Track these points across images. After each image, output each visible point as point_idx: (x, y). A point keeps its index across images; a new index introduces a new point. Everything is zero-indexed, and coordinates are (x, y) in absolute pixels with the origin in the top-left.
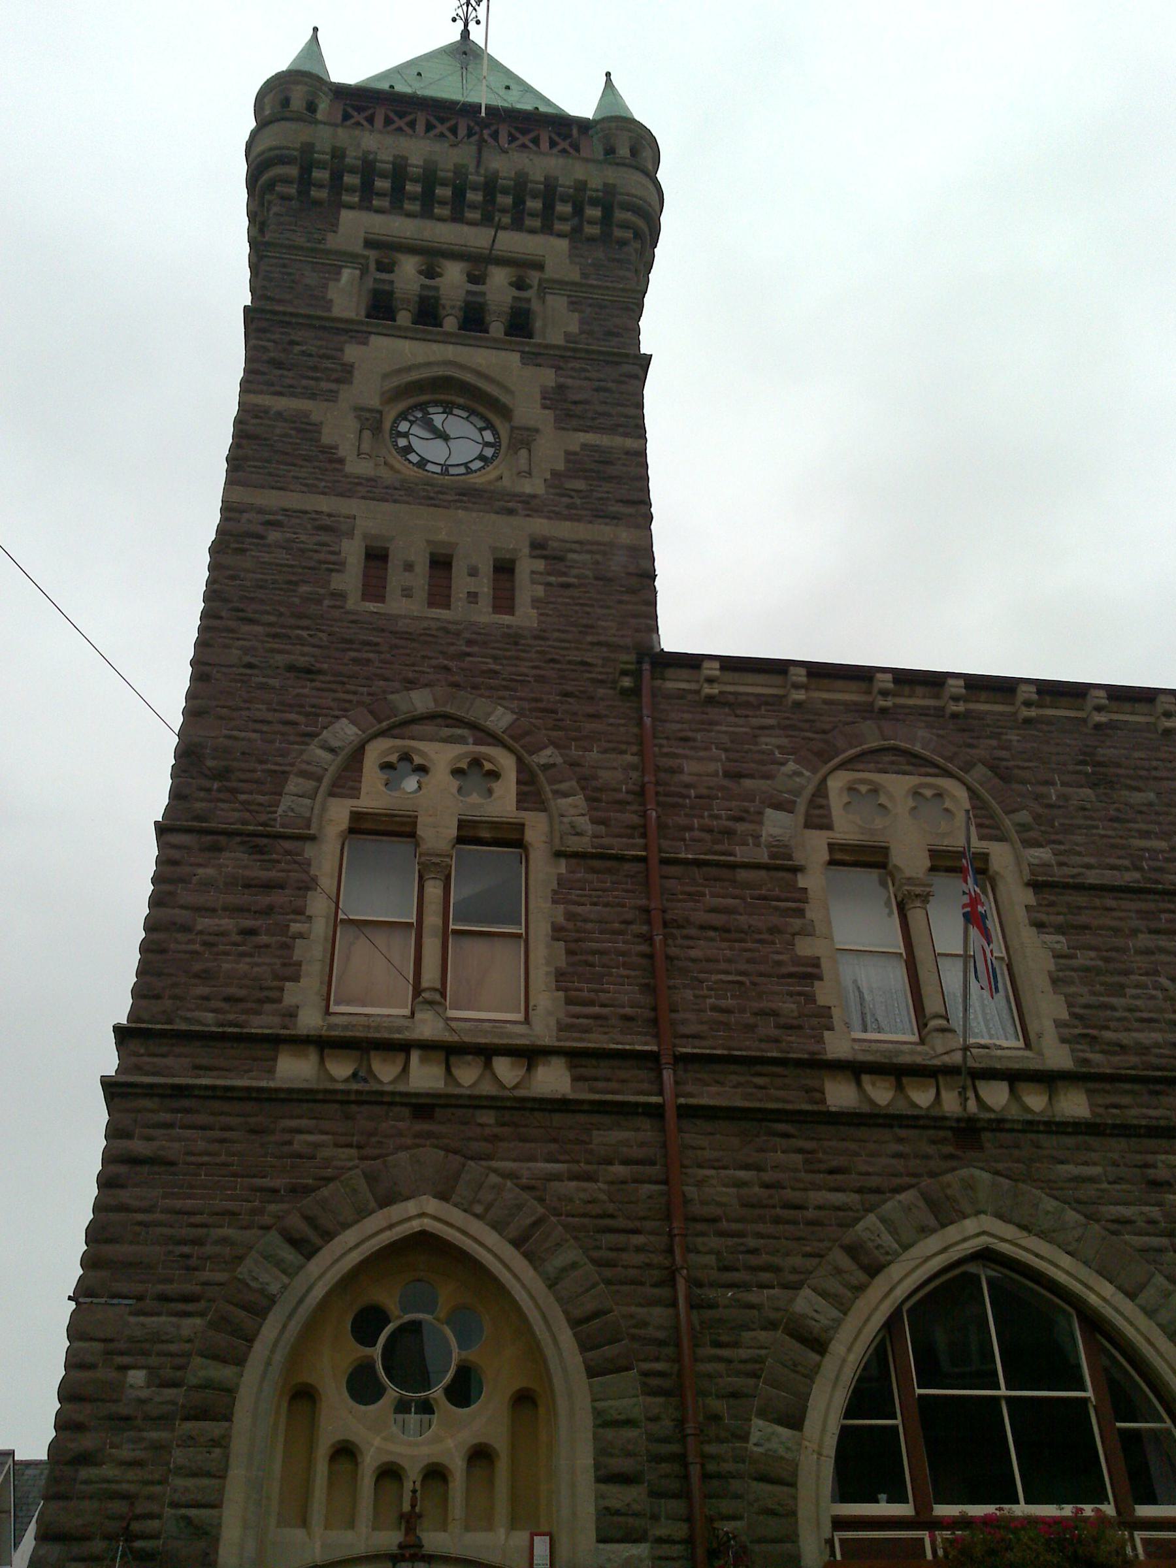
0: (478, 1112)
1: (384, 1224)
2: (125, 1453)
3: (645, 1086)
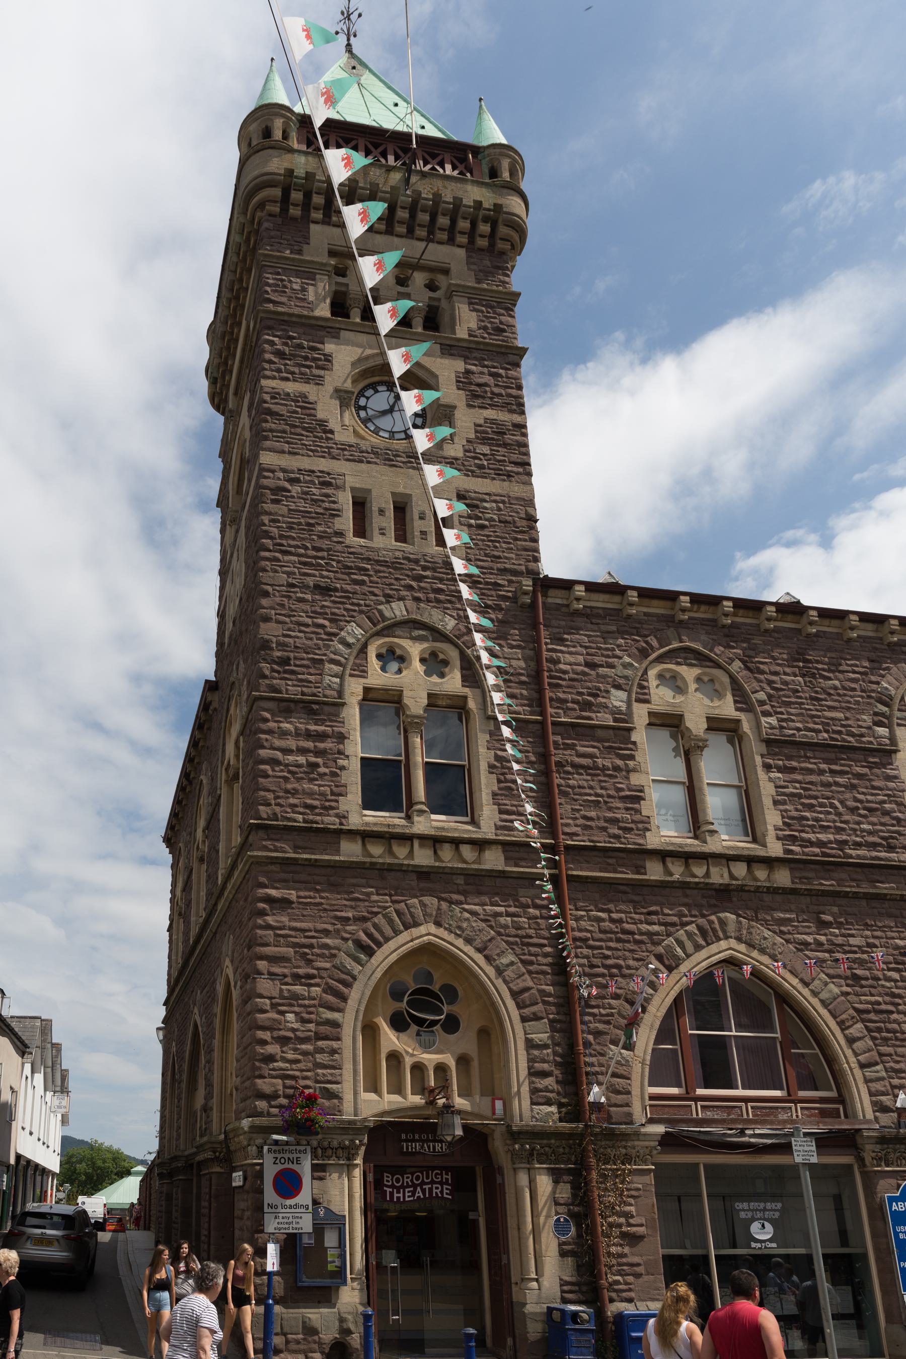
0: (454, 877)
1: (409, 939)
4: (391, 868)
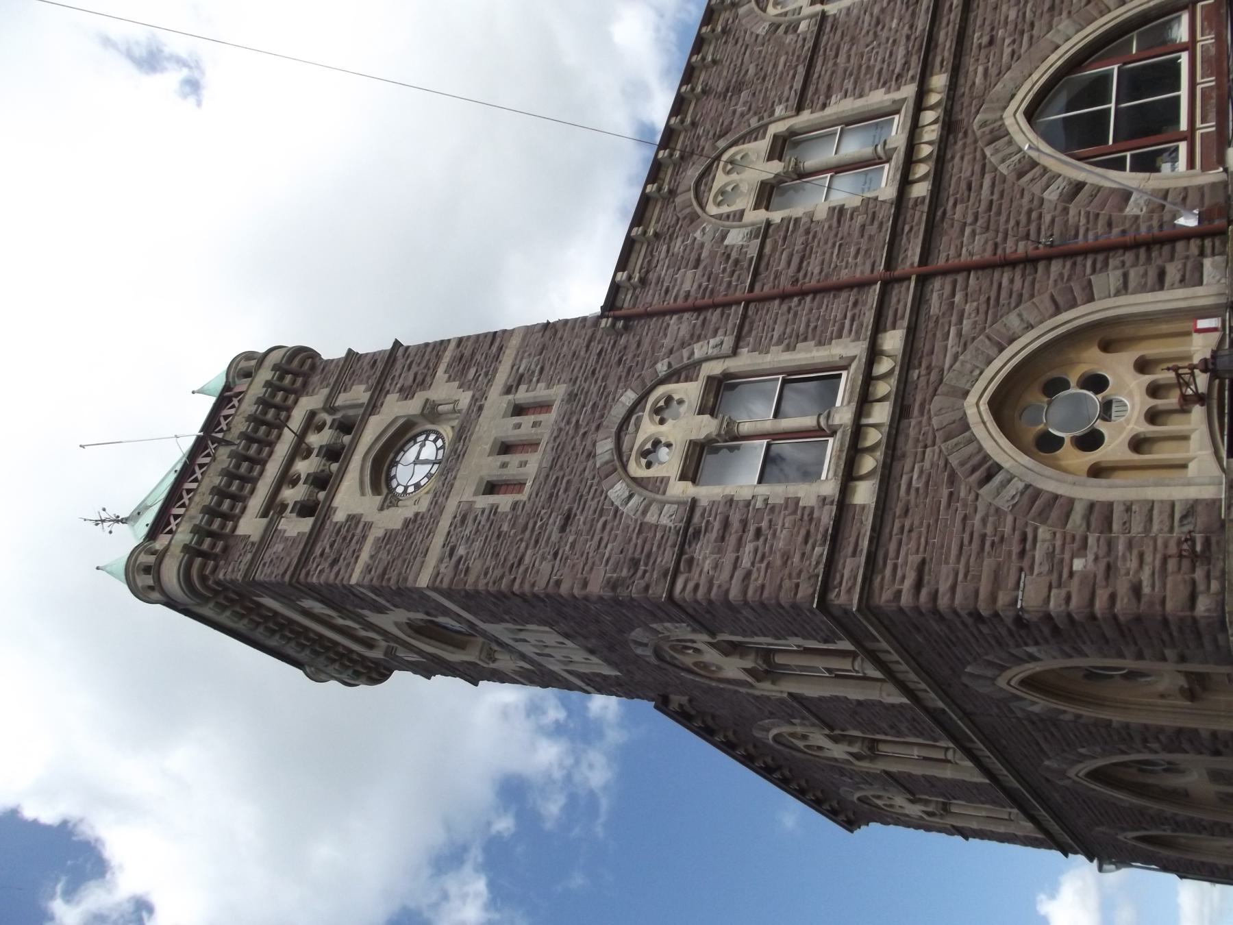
0: (910, 379)
2: (1133, 564)
3: (903, 289)
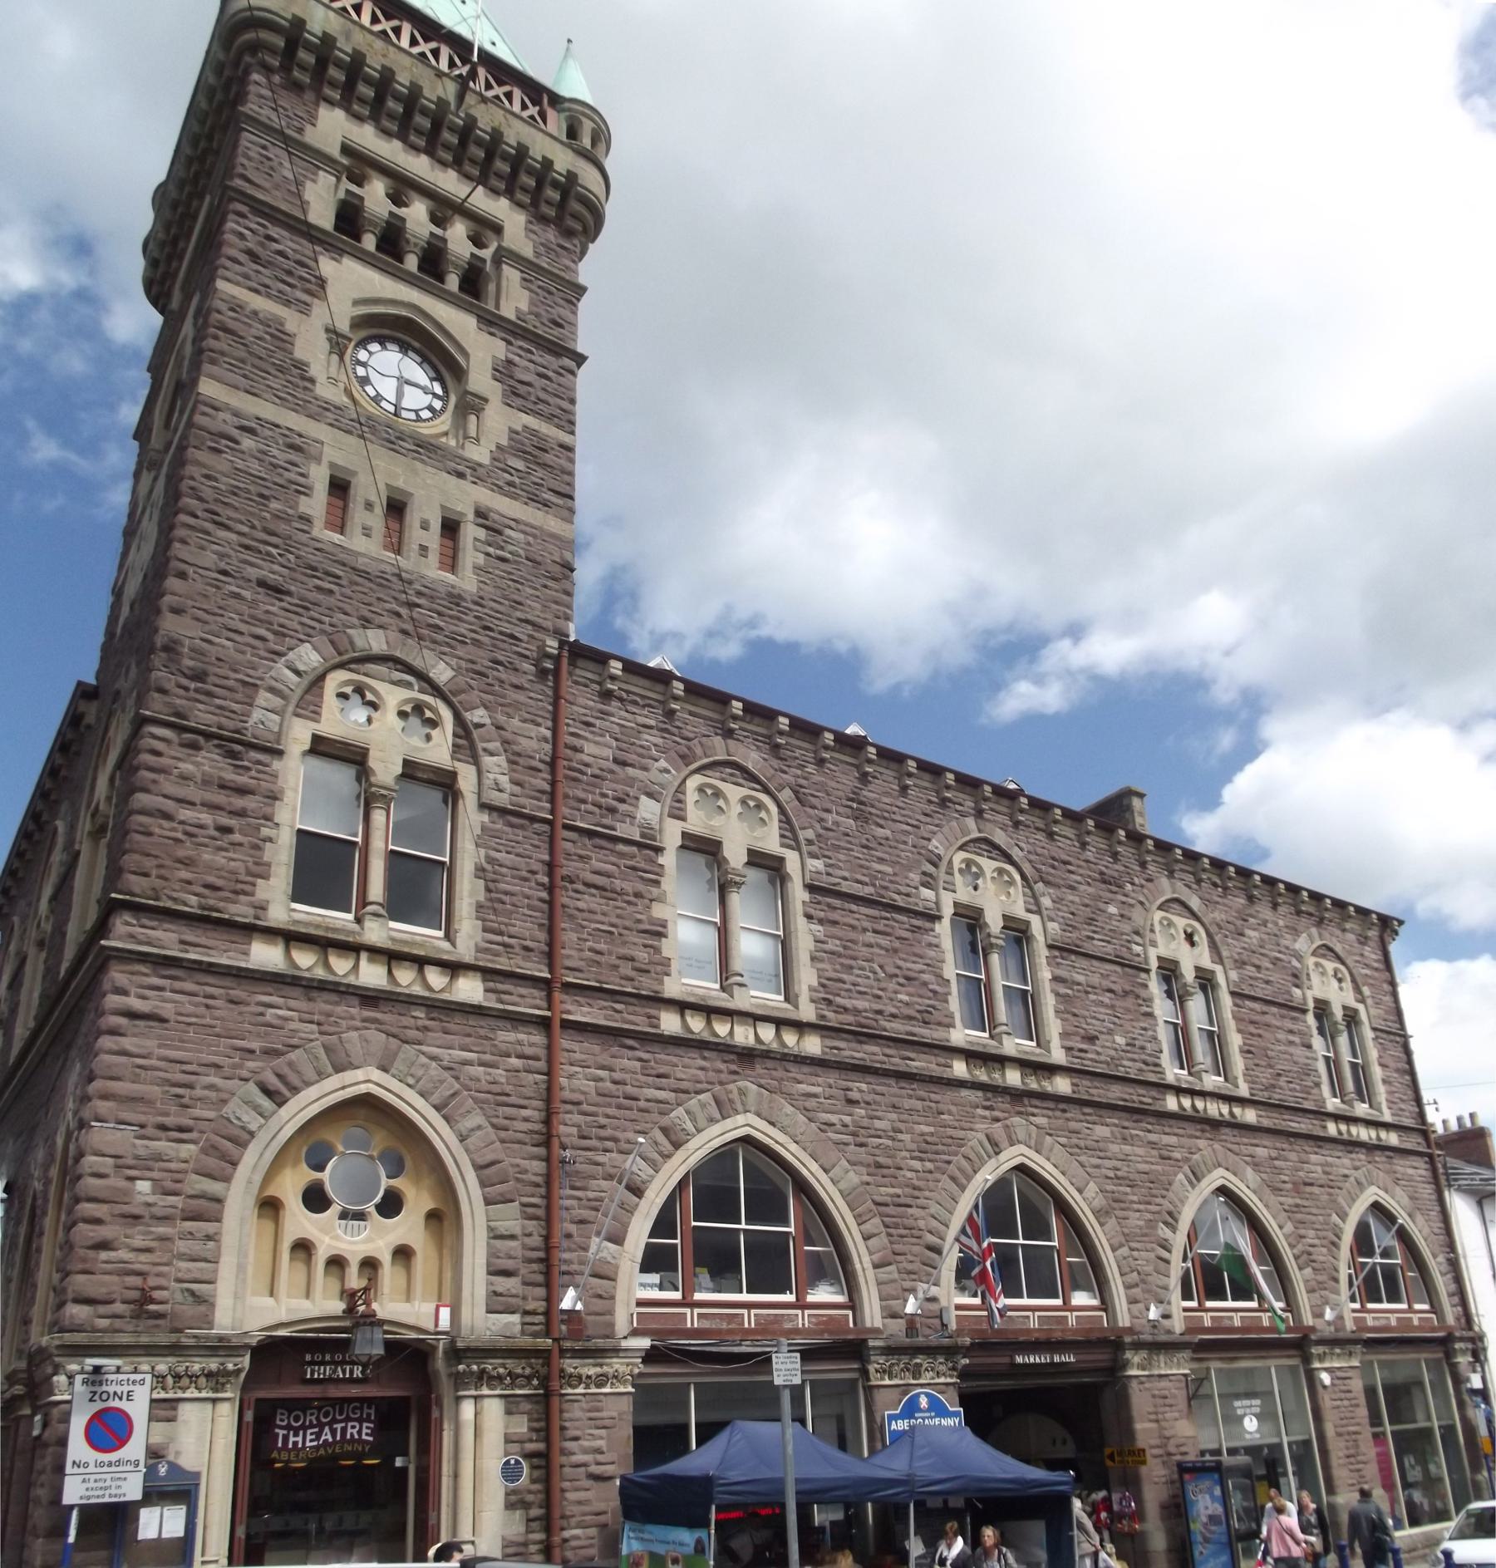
4: (323, 986)
